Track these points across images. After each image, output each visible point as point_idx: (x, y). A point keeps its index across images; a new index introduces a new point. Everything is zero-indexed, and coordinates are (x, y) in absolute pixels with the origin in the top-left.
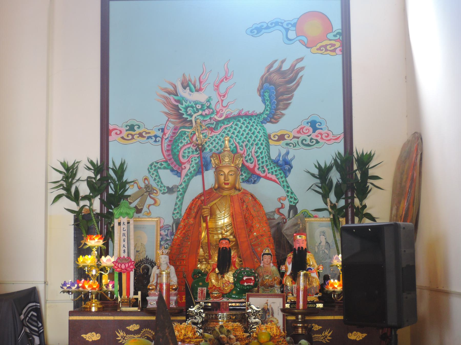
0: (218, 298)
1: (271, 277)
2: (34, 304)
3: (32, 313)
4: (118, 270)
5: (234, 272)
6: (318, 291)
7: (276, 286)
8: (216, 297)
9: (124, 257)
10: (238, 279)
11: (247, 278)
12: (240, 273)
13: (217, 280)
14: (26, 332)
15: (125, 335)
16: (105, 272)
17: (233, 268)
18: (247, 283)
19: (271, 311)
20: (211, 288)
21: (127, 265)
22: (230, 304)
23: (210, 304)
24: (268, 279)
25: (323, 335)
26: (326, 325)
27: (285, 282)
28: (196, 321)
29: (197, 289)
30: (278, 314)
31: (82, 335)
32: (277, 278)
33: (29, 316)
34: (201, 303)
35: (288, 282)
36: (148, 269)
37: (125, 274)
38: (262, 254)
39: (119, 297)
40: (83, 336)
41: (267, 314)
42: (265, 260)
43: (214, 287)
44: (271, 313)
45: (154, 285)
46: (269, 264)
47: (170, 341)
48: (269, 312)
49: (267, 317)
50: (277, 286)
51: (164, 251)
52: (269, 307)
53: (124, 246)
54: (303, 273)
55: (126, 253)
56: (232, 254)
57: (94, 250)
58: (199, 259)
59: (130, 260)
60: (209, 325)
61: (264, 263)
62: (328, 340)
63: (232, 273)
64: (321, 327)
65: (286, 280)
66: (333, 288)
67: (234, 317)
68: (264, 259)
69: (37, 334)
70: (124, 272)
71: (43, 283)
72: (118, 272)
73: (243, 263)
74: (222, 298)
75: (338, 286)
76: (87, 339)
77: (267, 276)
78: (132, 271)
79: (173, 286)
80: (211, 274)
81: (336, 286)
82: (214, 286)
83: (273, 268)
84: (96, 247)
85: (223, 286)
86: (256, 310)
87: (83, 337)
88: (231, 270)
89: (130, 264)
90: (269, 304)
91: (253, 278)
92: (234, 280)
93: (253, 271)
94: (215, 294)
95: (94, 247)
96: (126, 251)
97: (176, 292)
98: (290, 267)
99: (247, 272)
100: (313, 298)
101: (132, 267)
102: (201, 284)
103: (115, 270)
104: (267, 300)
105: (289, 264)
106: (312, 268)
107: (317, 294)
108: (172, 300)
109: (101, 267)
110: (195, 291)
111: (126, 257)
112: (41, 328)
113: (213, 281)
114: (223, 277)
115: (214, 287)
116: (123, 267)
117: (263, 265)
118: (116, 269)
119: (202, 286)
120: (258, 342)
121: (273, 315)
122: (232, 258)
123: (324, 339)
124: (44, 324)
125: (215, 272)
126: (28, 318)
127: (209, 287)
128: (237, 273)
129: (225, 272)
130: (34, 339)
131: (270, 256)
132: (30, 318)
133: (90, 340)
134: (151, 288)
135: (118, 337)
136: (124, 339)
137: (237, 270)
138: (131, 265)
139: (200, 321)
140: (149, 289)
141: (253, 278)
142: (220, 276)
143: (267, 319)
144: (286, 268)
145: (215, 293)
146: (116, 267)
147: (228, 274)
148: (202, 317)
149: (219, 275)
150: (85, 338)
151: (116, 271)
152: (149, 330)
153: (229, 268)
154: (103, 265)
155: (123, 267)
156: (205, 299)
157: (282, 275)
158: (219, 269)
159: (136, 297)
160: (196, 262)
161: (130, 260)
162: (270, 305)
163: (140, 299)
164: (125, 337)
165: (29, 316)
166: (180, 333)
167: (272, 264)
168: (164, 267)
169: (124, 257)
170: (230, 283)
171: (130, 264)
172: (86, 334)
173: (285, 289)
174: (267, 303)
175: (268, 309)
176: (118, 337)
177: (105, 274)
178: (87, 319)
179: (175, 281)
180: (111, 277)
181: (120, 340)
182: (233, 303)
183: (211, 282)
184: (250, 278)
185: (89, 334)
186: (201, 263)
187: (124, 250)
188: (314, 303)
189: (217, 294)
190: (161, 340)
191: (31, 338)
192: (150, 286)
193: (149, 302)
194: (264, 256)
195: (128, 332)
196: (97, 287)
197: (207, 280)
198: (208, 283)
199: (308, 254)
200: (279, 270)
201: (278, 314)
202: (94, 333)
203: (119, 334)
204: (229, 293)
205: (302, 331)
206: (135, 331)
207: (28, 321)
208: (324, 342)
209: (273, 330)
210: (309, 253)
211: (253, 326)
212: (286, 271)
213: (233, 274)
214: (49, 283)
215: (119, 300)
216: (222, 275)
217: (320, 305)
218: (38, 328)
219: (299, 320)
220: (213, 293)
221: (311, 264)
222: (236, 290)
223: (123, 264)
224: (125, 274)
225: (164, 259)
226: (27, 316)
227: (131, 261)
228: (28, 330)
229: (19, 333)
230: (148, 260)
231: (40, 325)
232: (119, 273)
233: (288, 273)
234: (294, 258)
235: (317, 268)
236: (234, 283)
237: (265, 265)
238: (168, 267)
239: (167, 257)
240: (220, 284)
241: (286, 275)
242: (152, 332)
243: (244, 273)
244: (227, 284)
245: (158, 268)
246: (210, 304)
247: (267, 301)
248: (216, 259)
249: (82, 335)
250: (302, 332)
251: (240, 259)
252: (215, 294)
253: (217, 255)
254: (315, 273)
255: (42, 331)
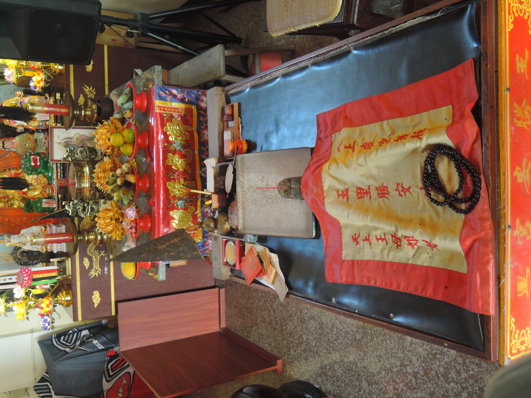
0: (53, 189)
1: (26, 142)
2: (54, 340)
3: (62, 341)
4: (30, 282)
5: (25, 174)
6: (43, 97)
7: (35, 137)
8: (53, 190)
9: (16, 279)
10: (34, 170)
11: (32, 162)
12: (27, 168)
13: (35, 190)
14: (80, 345)
15: (94, 270)
16: (30, 293)
17: (22, 175)
18: (37, 162)
19: (66, 140)
20: (43, 195)
21: (25, 275)
22: (59, 177)
23: (60, 196)
24: (29, 144)
25: (88, 93)
26: (79, 90)
27: (35, 127)
28: (81, 208)
29: (44, 208)
30: (70, 133)
31: (96, 307)
32: (26, 136)
33: (65, 343)
34: (64, 204)
35: (33, 125)
36: (24, 252)
37: (34, 276)
38: (3, 149)
39: (57, 278)
40: (96, 306)
41: (70, 143)
42: (9, 147)
43: (43, 192)
44: (69, 140)
45: (42, 247)
46: (13, 143)
47: (172, 242)
48: (69, 141)
49: (73, 143)
50: (36, 135)
51: (7, 240)
52: (63, 142)
53: (5, 280)
54: (30, 106)
55: (12, 277)
56: (7, 176)
57: (8, 306)
58: (8, 207)
59: (19, 273)
60: (86, 196)
61: (12, 148)
62: (93, 89)
63: (27, 176)
64: (81, 95)
65: (32, 126)
66: (42, 81)
67: (79, 173)
68: (9, 148)
69: (80, 333)
70: (32, 277)
71: (32, 334)
72: (32, 282)
73: (12, 167)
74: (52, 185)
75: (40, 76)
76: (99, 302)
77: (25, 145)
78: (30, 270)
79: (42, 230)
80: (29, 195)
81: (39, 78)
82: (41, 192)
83: (17, 139)
84: (5, 304)
85: (41, 184)
86: (69, 153)
87: (97, 306)
88: (24, 177)
89: (24, 273)
90: (60, 142)
91: (32, 157)
92: (34, 174)
93: (24, 156)
94: (49, 191)
95: (5, 306)
96: (10, 277)
97: (47, 226)
98: (19, 122)
99: (26, 162)
100: (51, 101)
101: (27, 270)
102: (39, 205)
103: (30, 285)
104: (56, 143)
105: (15, 123)
106: (20, 101)
107: (46, 98)
108: (56, 231)
109: (25, 297)
110: (45, 210)
111: (16, 277)
112: (73, 330)
113: (36, 193)
114: (31, 184)
115: (43, 192)
116: (27, 278)
117: (14, 148)
118: (29, 284)
119: (41, 203)
120: (122, 146)
121: (71, 138)
122: (12, 176)
123: (92, 93)
124: (68, 328)
125: (27, 192)
126: (67, 344)
127: (42, 197)
128: (27, 172)
129: (26, 183)
130: (84, 336)
131: (5, 142)
132: (67, 342)
133: (100, 299)
134: (45, 250)
135: (96, 275)
136: (97, 270)
137: (24, 171)
138: (25, 271)
139: (82, 205)
140: (46, 251)
141: (32, 157)
142: (31, 187)
143: (75, 144)
144: (19, 126)
145: (48, 191)
146: (27, 285)
147: (28, 180)
148: (77, 203)
149: (30, 188)
150: (97, 304)
151: (30, 284)
152: (88, 249)
153: (22, 179)
154: (23, 295)
155: (27, 278)
156: (54, 200)
157: (26, 130)
158: (24, 188)
159: (56, 263)
160: (11, 209)
161: (19, 273)
162: (61, 140)
163: (58, 259)
164: (95, 270)
165: (65, 343)
166: (109, 224)
167: (13, 141)
168: (22, 239)
169: (16, 279)
170: (37, 178)
171: (24, 273)
172: (94, 303)
173: (40, 128)
174: (59, 143)
175: (66, 142)
176: (96, 275)
177: (32, 292)
178: (80, 305)
179: (37, 228)
180: (34, 287)
181: (98, 274)
182: (55, 175)
183: (37, 195)
184: (477, 28)
185: (94, 301)
186: (12, 205)
187: (9, 279)
188: (55, 101)
189: (49, 190)
190: (172, 254)
191: (85, 338)
192: (43, 250)
193: (59, 250)
194: (5, 147)
195: (91, 267)
196: (48, 299)
197: (35, 199)
198: (38, 198)
199: (4, 105)
200: (21, 133)
201: (70, 133)
202: (93, 297)
203: (92, 275)
204: (47, 179)
205: (88, 111)
206: (89, 261)
207: (70, 343)
208: (95, 93)
209: (104, 132)
210: (2, 104)
211: (84, 156)
212: (23, 126)
213: (28, 175)
214: (31, 328)
215: (59, 278)
216: (30, 185)
217: (58, 96)
218: (74, 333)
219: (83, 112)
220: (48, 193)
221: (14, 102)
222: (44, 172)
223: (24, 279)
224: (34, 276)
225: (15, 240)
226: (65, 345)
227: (21, 272)
228: (78, 343)
229: (84, 351)
230: (13, 253)
231: (71, 332)
232: (33, 281)
233: (25, 124)
234: (9, 118)
235: (19, 97)
236: (38, 174)
237: (14, 147)
238: (23, 235)
239: (12, 237)
240: (39, 187)
241: (27, 126)
242: (90, 246)
243: (27, 165)
244: (39, 181)
245: (25, 244)
246: (60, 196)
247: (56, 143)
248: (12, 191)
249: (96, 307)
250: (90, 111)
251: (7, 170)
252: (49, 191)
253: (8, 191)
254: (24, 99)
255: (76, 329)
